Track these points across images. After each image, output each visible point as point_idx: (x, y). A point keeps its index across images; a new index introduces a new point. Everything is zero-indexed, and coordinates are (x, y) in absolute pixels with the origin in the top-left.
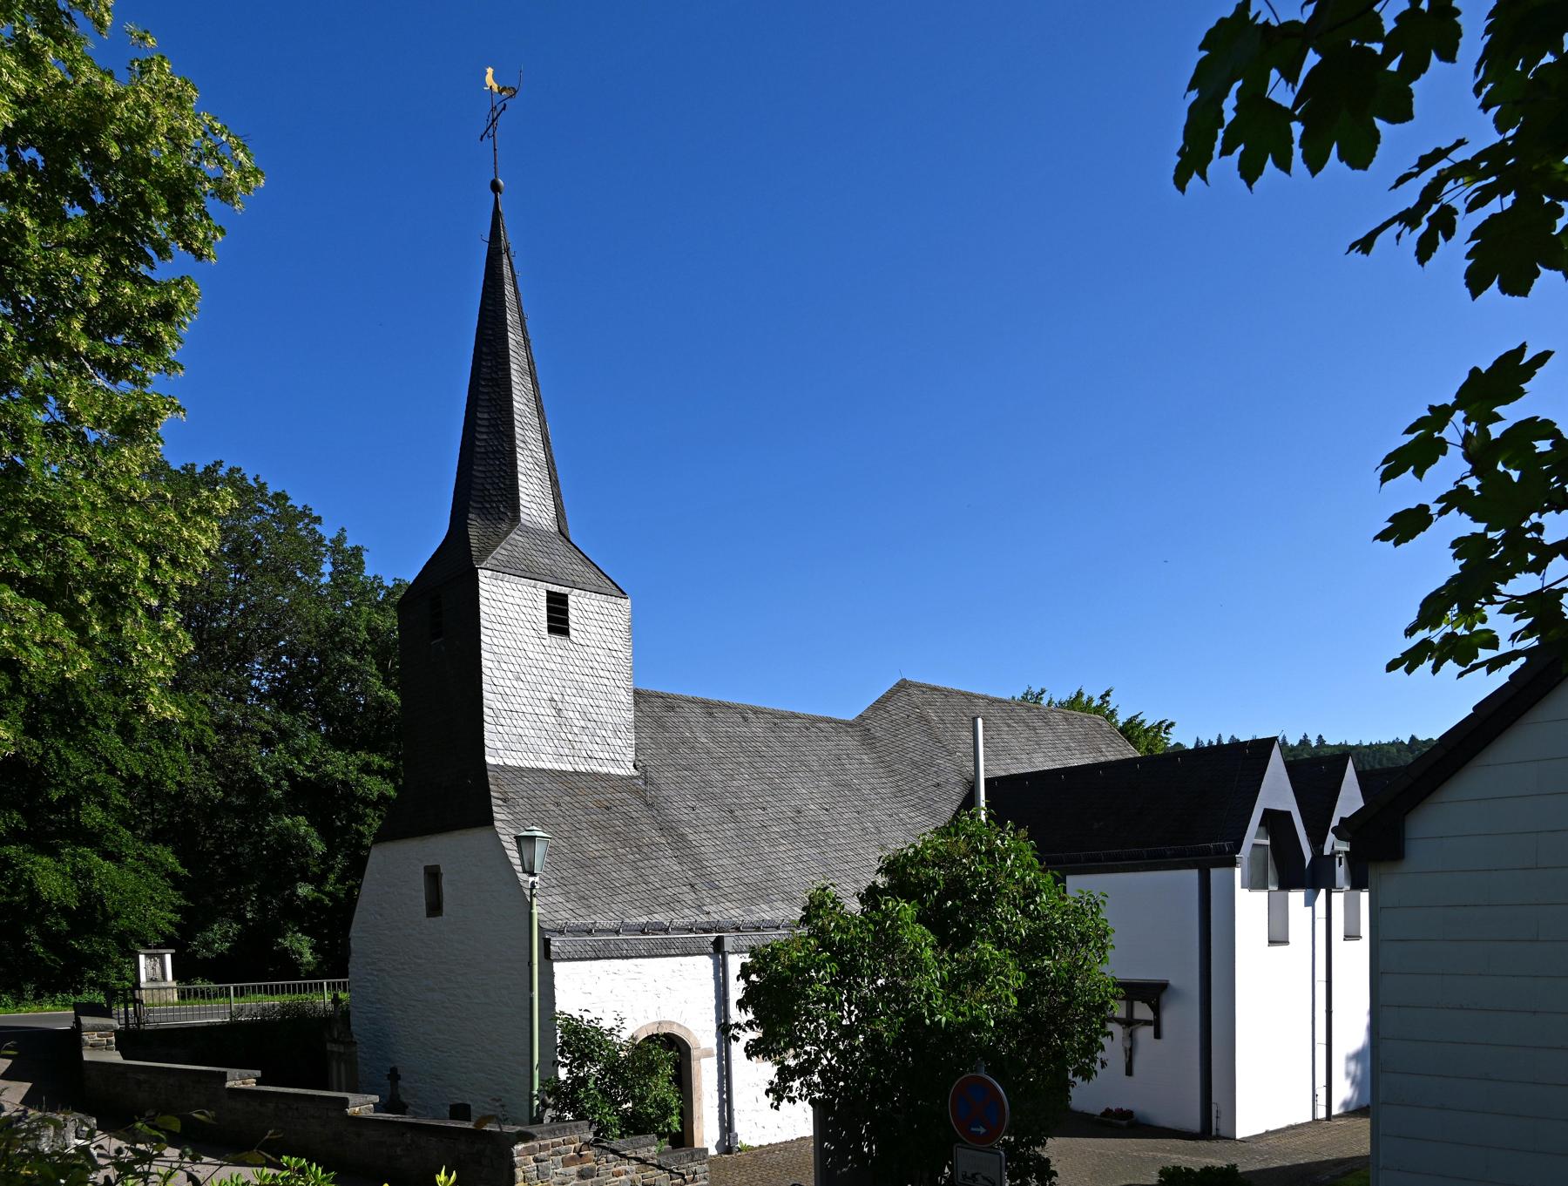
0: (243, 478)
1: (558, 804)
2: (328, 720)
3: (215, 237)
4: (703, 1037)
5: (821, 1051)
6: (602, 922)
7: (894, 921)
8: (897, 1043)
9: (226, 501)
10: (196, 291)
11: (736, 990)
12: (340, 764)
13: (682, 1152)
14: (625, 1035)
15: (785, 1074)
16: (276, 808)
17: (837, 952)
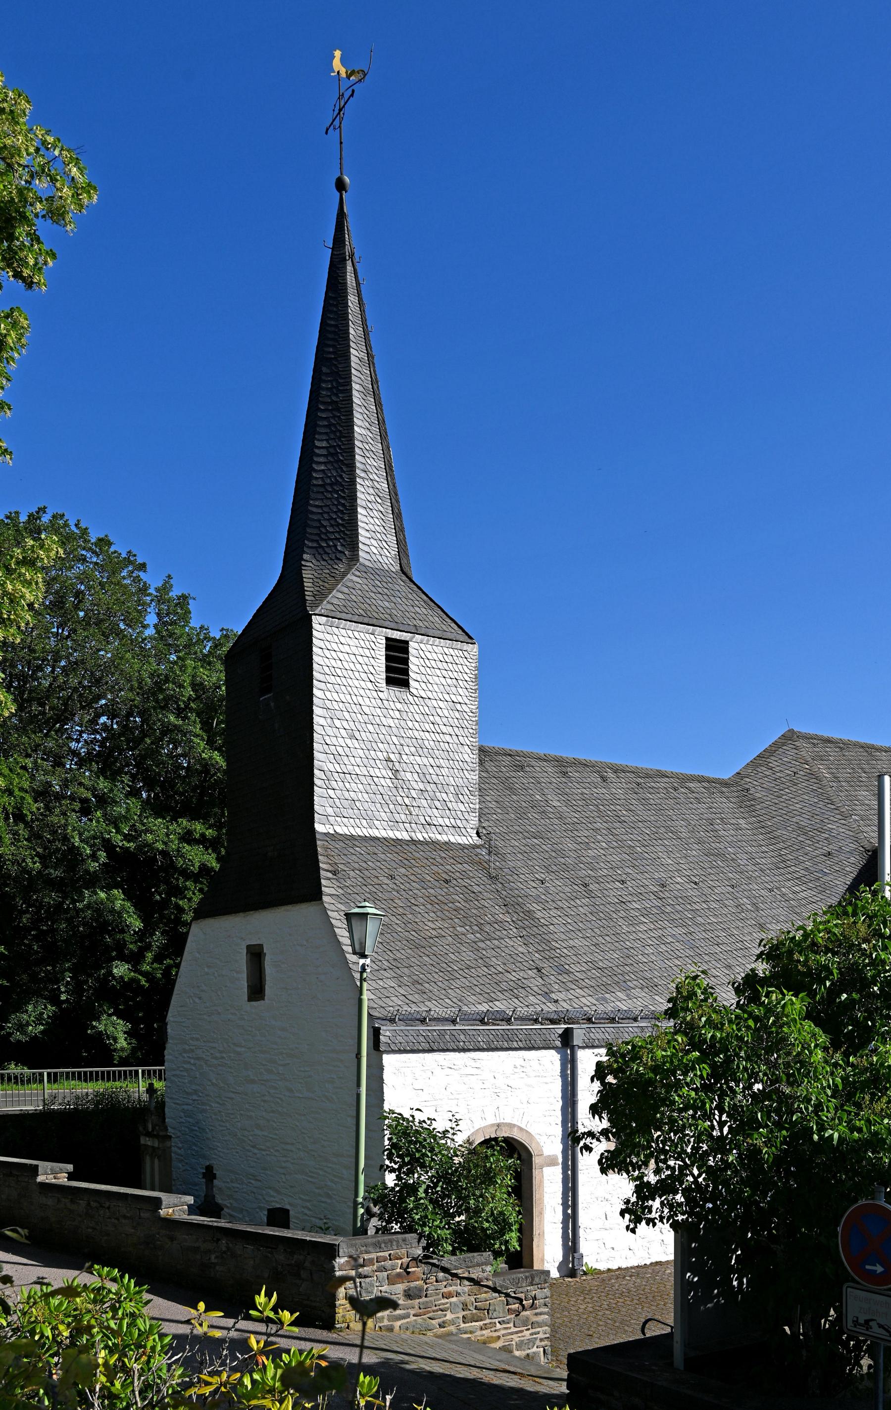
0: (66, 525)
1: (392, 877)
2: (150, 784)
3: (46, 263)
4: (547, 1141)
5: (686, 1166)
6: (438, 1010)
7: (778, 1018)
8: (778, 1161)
9: (52, 550)
10: (25, 323)
11: (588, 1092)
12: (161, 833)
13: (520, 1274)
14: (460, 1139)
15: (644, 1191)
16: (92, 881)
17: (708, 1050)
